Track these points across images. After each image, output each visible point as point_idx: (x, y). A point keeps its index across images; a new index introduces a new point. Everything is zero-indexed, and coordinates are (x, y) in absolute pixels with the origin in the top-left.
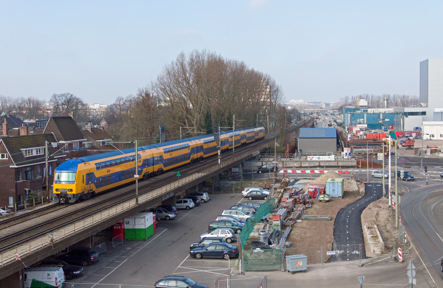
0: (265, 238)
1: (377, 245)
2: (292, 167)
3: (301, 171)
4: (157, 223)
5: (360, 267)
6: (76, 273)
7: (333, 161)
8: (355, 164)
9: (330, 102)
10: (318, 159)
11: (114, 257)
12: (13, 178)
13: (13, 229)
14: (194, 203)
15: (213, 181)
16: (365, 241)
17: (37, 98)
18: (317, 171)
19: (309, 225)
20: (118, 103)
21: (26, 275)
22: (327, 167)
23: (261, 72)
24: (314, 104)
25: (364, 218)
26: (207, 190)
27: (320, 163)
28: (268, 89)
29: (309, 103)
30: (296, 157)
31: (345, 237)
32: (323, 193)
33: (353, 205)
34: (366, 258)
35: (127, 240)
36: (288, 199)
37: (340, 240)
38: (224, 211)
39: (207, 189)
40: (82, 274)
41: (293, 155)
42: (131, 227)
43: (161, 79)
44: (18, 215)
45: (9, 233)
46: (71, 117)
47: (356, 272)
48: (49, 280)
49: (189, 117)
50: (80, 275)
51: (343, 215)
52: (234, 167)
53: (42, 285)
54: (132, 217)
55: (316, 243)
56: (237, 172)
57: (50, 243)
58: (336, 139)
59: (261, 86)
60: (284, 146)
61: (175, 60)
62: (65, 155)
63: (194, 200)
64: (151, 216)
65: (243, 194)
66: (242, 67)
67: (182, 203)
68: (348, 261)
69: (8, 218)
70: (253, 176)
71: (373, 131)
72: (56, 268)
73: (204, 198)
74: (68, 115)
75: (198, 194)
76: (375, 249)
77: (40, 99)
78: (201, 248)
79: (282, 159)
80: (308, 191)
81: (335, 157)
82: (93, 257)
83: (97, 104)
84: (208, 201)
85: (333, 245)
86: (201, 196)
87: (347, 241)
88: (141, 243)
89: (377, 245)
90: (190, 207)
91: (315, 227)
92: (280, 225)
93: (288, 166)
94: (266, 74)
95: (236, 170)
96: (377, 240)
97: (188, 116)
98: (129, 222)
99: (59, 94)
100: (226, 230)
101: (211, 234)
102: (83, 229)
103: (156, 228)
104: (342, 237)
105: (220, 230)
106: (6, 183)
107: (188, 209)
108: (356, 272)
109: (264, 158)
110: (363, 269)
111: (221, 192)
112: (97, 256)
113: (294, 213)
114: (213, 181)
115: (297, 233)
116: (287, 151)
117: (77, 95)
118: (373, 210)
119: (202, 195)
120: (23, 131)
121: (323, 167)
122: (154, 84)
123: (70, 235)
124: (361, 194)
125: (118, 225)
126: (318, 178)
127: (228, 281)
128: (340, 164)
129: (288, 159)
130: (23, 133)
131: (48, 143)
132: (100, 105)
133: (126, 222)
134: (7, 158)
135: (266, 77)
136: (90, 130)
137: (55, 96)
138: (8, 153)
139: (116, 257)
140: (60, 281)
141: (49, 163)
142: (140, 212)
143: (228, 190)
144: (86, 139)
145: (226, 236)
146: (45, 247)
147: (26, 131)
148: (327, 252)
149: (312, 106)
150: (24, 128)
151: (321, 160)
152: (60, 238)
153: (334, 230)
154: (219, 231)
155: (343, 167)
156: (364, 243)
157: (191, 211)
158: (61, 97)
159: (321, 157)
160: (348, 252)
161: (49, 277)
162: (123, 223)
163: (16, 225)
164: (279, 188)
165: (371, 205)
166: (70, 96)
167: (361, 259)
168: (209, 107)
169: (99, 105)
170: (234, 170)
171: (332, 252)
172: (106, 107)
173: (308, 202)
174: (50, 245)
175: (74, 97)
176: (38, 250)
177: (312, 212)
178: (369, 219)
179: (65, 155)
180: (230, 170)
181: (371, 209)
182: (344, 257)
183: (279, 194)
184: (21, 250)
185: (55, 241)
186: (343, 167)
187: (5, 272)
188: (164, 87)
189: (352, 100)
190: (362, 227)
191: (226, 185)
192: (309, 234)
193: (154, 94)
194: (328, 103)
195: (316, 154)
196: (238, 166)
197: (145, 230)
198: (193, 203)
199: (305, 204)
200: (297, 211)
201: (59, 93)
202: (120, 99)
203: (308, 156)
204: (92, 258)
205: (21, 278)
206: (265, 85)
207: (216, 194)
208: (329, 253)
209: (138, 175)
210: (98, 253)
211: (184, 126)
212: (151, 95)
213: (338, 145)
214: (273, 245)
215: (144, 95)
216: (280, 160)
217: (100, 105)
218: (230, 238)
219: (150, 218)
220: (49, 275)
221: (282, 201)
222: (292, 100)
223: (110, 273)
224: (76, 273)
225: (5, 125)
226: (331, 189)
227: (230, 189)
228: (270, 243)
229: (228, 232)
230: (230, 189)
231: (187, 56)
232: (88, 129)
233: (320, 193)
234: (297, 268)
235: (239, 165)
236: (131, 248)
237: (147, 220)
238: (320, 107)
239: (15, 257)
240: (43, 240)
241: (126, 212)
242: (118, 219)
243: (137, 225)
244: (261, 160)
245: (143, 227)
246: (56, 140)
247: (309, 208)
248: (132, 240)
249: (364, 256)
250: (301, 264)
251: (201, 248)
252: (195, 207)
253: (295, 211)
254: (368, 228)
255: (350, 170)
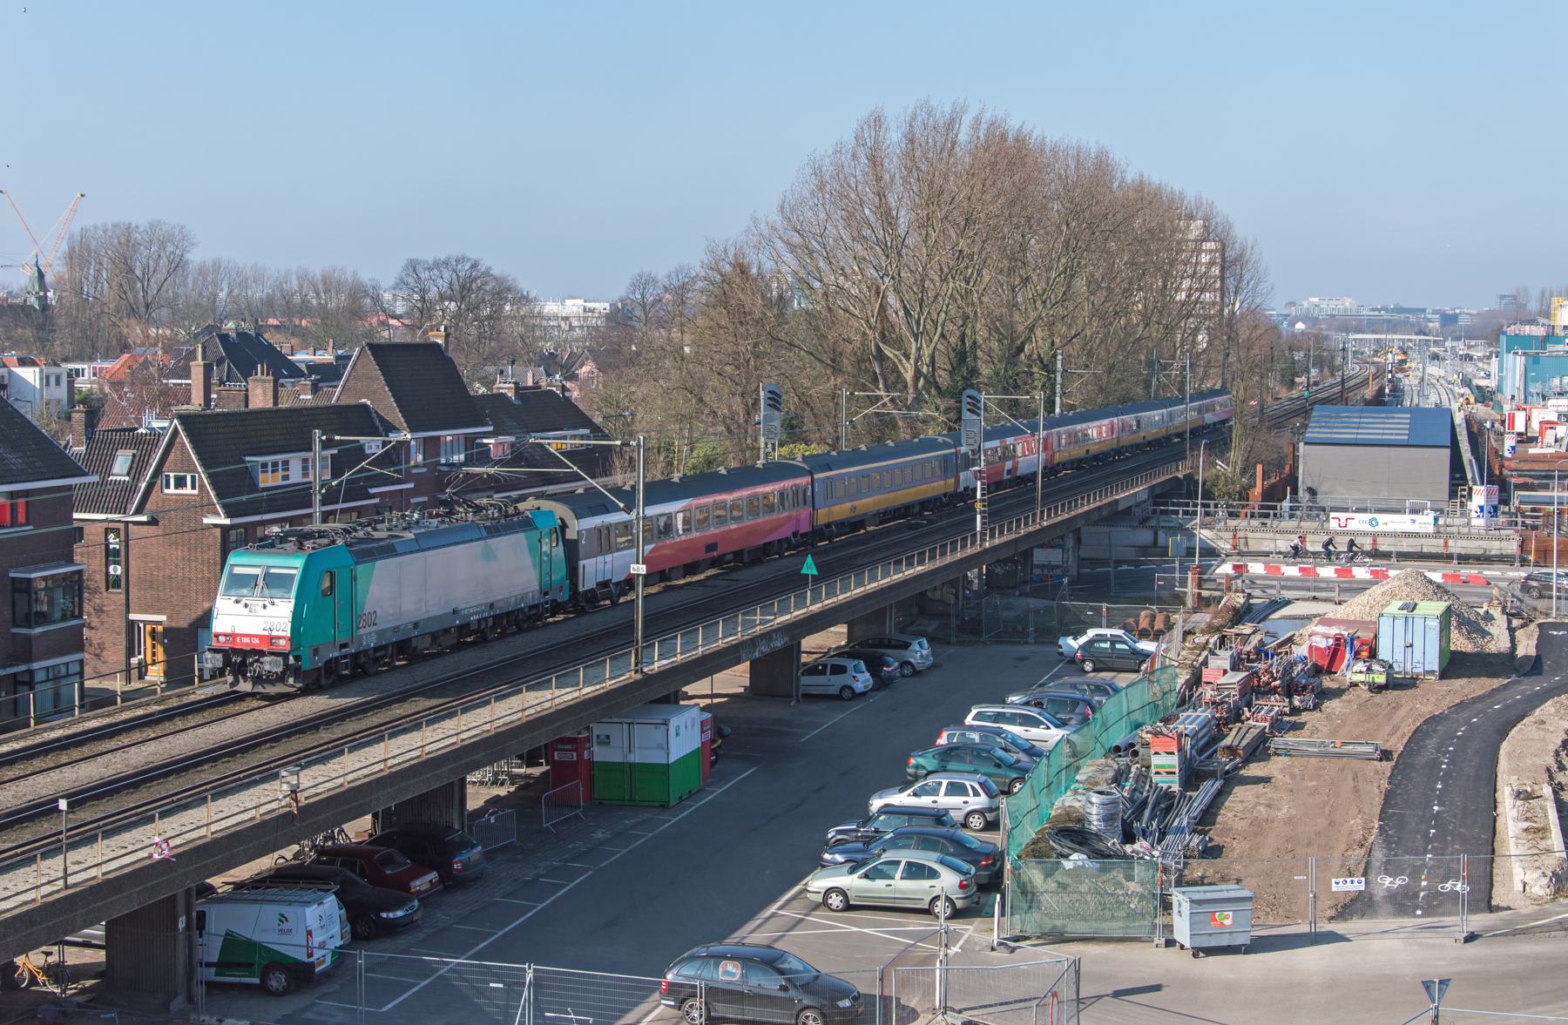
0: (1108, 819)
1: (1537, 864)
2: (1267, 554)
3: (1301, 570)
4: (719, 747)
5: (1458, 944)
6: (391, 915)
7: (1427, 536)
8: (1512, 547)
9: (1458, 311)
10: (1371, 524)
11: (540, 864)
12: (215, 564)
13: (168, 746)
14: (872, 675)
15: (956, 595)
16: (1496, 845)
17: (355, 274)
18: (1360, 573)
19: (1293, 776)
20: (639, 297)
21: (202, 916)
22: (1404, 556)
23: (1177, 189)
24: (1396, 316)
25: (1509, 755)
26: (930, 629)
27: (1379, 540)
28: (1203, 255)
29: (1376, 313)
30: (1286, 515)
31: (1424, 827)
32: (1365, 654)
33: (1480, 706)
34: (1491, 912)
35: (600, 803)
36: (1225, 672)
37: (1399, 838)
38: (974, 711)
39: (932, 626)
40: (413, 922)
41: (1275, 508)
42: (618, 759)
43: (793, 210)
44: (203, 697)
45: (151, 759)
46: (437, 344)
47: (1441, 963)
48: (284, 939)
49: (891, 355)
50: (405, 926)
51: (1431, 743)
52: (1043, 546)
53: (260, 953)
54: (620, 720)
55: (1309, 844)
56: (1058, 567)
57: (289, 805)
58: (1448, 450)
59: (1179, 243)
60: (1244, 472)
61: (849, 138)
62: (411, 485)
63: (875, 665)
64: (693, 720)
65: (1060, 647)
66: (1102, 167)
67: (825, 674)
68: (1419, 916)
69: (162, 707)
70: (1113, 582)
71: (900, 423)
72: (309, 895)
73: (912, 660)
74: (428, 338)
75: (893, 642)
76: (1531, 876)
77: (365, 277)
78: (860, 845)
79: (1232, 523)
80: (1311, 647)
81: (1436, 519)
82: (460, 862)
83: (575, 298)
84: (929, 668)
85: (1369, 856)
86: (903, 652)
87: (1427, 839)
88: (649, 816)
89: (1537, 864)
90: (857, 691)
91: (1314, 783)
92: (1177, 771)
93: (1253, 547)
94: (1198, 199)
95: (1054, 556)
96: (1542, 845)
97: (888, 351)
98: (608, 737)
99: (430, 259)
100: (967, 784)
101: (909, 795)
102: (419, 757)
103: (713, 764)
104: (1414, 824)
105: (945, 782)
106: (190, 579)
107: (847, 695)
108: (1441, 963)
109: (1163, 517)
110: (1473, 949)
111: (984, 639)
112: (477, 857)
113: (1240, 728)
114: (956, 595)
115: (1242, 802)
116: (1258, 490)
117: (498, 264)
118: (1552, 729)
119: (906, 646)
120: (259, 391)
121: (1386, 555)
122: (763, 227)
123: (366, 776)
124: (1520, 666)
125: (569, 747)
126: (1362, 598)
127: (938, 971)
128: (1456, 547)
129: (1255, 523)
130: (261, 398)
131: (324, 438)
132: (585, 301)
133: (598, 737)
134: (193, 487)
135: (1198, 208)
136: (511, 394)
137: (413, 266)
138: (198, 473)
139: (548, 863)
140: (324, 942)
141: (310, 505)
142: (651, 702)
143: (1010, 630)
144: (491, 429)
145: (966, 802)
146: (267, 817)
147: (271, 394)
148: (1334, 880)
149: (1389, 321)
150: (264, 381)
151: (1381, 528)
152: (329, 785)
153: (1388, 797)
154: (940, 784)
155: (1464, 559)
156: (1493, 851)
157: (857, 706)
158: (436, 271)
159: (1381, 518)
160: (1424, 883)
161: (285, 926)
162: (588, 739)
163: (183, 735)
164: (1203, 632)
165: (1549, 707)
166: (467, 267)
167: (1463, 914)
168: (966, 318)
169: (581, 302)
170: (1040, 556)
171: (1352, 882)
172: (608, 311)
173: (1304, 688)
174: (288, 809)
175: (483, 269)
176: (238, 828)
177: (1319, 726)
178: (1529, 761)
179: (411, 485)
180: (1028, 554)
181: (1543, 722)
182: (1402, 903)
183: (1199, 655)
184: (179, 823)
185: (306, 798)
186: (1464, 559)
187: (110, 900)
188: (801, 240)
189: (1542, 304)
190: (1495, 791)
191: (1005, 614)
192: (1285, 811)
193: (759, 262)
194: (1451, 312)
195: (1364, 506)
196: (1060, 541)
197: (665, 769)
198: (867, 675)
199: (1290, 696)
200: (1257, 721)
201: (429, 257)
202: (643, 282)
203: (1333, 515)
204: (456, 863)
205: (181, 925)
206: (1195, 241)
207: (962, 643)
208: (1341, 884)
209: (644, 566)
210: (480, 848)
211: (872, 387)
212: (754, 271)
213: (1458, 476)
214: (1137, 846)
215: (727, 268)
216: (1222, 524)
217: (585, 301)
218: (981, 812)
219: (689, 726)
220: (283, 918)
221: (1204, 680)
222: (1312, 299)
223: (518, 922)
224: (391, 915)
225: (201, 369)
226: (1400, 644)
227: (1020, 628)
228: (1129, 838)
229: (973, 787)
230: (1020, 628)
231: (893, 125)
232: (503, 391)
233: (1357, 656)
234: (1210, 934)
235: (1062, 537)
236: (608, 835)
237: (678, 734)
238: (1417, 329)
239: (151, 849)
240: (266, 793)
241: (590, 699)
242: (559, 724)
243: (637, 752)
244: (1153, 523)
245: (657, 758)
246: (377, 428)
247: (1306, 709)
248: (619, 803)
249: (1483, 899)
250: (1228, 922)
251: (860, 845)
252: (877, 690)
253: (1248, 719)
254: (1518, 795)
255: (1490, 572)
